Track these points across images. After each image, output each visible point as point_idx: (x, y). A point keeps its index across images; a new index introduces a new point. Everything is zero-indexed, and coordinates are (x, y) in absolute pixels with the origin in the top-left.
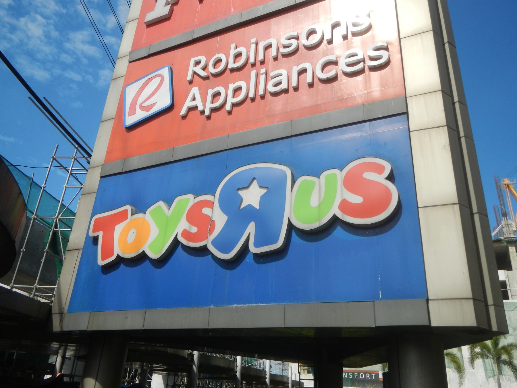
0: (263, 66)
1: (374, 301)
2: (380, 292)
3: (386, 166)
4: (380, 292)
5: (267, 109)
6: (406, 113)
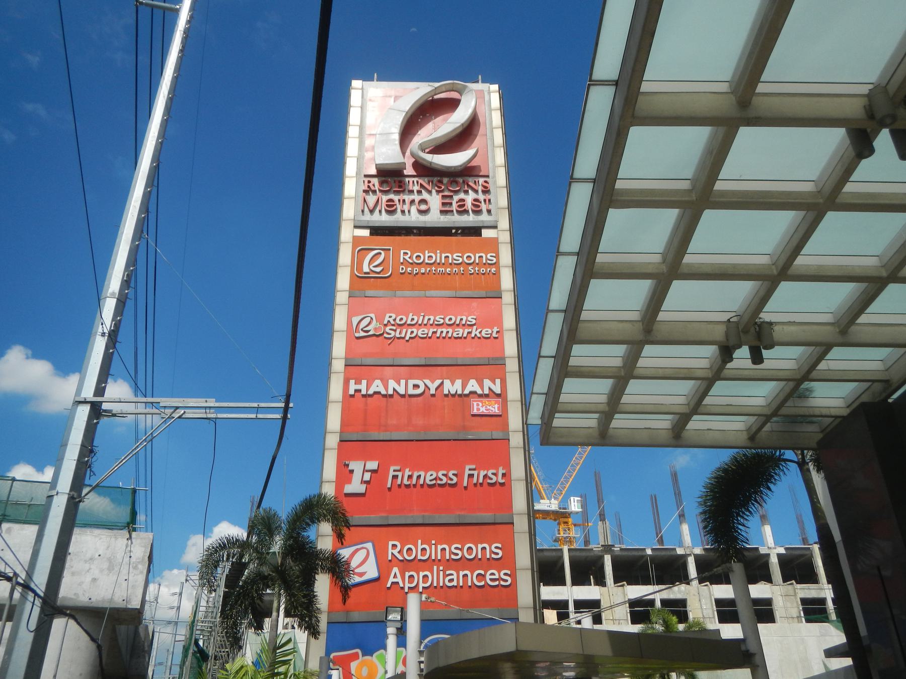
0: (425, 327)
3: (484, 546)
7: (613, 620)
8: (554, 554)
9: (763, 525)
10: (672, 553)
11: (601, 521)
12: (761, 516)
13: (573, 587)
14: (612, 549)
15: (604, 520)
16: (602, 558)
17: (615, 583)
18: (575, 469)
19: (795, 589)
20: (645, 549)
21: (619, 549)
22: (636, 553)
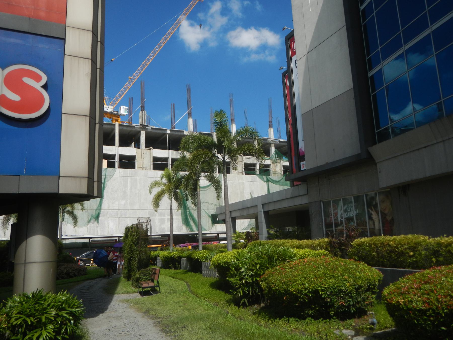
1: (19, 175)
2: (25, 169)
3: (43, 77)
4: (25, 169)
5: (227, 272)
6: (64, 39)
7: (142, 168)
8: (109, 127)
9: (232, 124)
10: (182, 134)
11: (141, 110)
12: (231, 119)
13: (120, 147)
14: (147, 127)
15: (144, 110)
16: (139, 132)
17: (146, 148)
18: (126, 91)
19: (242, 158)
20: (166, 130)
21: (151, 128)
22: (161, 132)
